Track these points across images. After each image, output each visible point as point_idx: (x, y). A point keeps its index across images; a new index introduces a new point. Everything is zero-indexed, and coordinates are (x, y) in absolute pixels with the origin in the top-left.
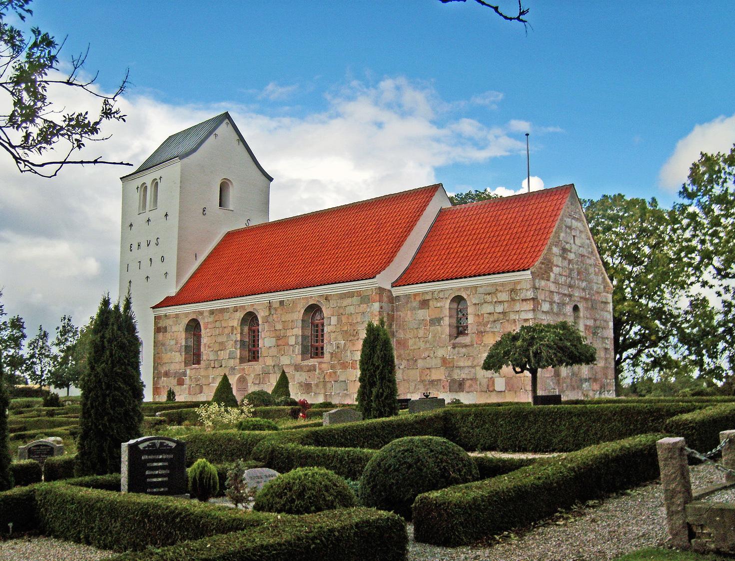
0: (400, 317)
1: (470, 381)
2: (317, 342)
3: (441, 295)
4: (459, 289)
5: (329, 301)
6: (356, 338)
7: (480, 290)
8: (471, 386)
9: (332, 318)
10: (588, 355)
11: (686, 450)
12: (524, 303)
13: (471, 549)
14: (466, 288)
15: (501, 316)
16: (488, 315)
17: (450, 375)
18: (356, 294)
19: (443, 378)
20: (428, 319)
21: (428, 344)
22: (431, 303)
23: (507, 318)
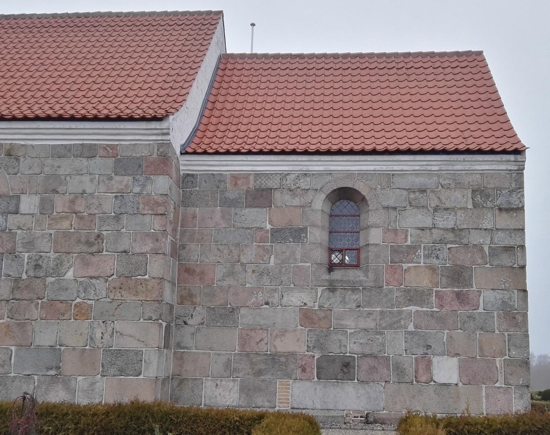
0: (194, 217)
1: (369, 360)
2: (24, 245)
3: (304, 184)
4: (350, 175)
5: (17, 159)
6: (94, 249)
7: (399, 182)
8: (373, 369)
9: (23, 197)
10: (492, 300)
11: (166, 239)
12: (505, 215)
13: (228, 414)
14: (363, 175)
15: (450, 236)
16: (419, 232)
17: (319, 345)
18: (101, 152)
19: (301, 349)
20: (269, 227)
21: (265, 278)
22: (277, 195)
23: (465, 241)
